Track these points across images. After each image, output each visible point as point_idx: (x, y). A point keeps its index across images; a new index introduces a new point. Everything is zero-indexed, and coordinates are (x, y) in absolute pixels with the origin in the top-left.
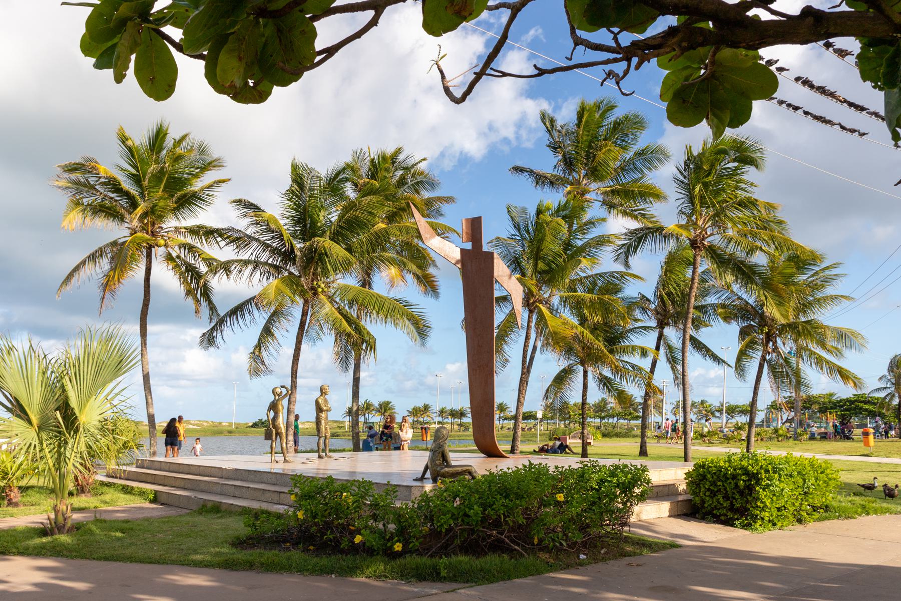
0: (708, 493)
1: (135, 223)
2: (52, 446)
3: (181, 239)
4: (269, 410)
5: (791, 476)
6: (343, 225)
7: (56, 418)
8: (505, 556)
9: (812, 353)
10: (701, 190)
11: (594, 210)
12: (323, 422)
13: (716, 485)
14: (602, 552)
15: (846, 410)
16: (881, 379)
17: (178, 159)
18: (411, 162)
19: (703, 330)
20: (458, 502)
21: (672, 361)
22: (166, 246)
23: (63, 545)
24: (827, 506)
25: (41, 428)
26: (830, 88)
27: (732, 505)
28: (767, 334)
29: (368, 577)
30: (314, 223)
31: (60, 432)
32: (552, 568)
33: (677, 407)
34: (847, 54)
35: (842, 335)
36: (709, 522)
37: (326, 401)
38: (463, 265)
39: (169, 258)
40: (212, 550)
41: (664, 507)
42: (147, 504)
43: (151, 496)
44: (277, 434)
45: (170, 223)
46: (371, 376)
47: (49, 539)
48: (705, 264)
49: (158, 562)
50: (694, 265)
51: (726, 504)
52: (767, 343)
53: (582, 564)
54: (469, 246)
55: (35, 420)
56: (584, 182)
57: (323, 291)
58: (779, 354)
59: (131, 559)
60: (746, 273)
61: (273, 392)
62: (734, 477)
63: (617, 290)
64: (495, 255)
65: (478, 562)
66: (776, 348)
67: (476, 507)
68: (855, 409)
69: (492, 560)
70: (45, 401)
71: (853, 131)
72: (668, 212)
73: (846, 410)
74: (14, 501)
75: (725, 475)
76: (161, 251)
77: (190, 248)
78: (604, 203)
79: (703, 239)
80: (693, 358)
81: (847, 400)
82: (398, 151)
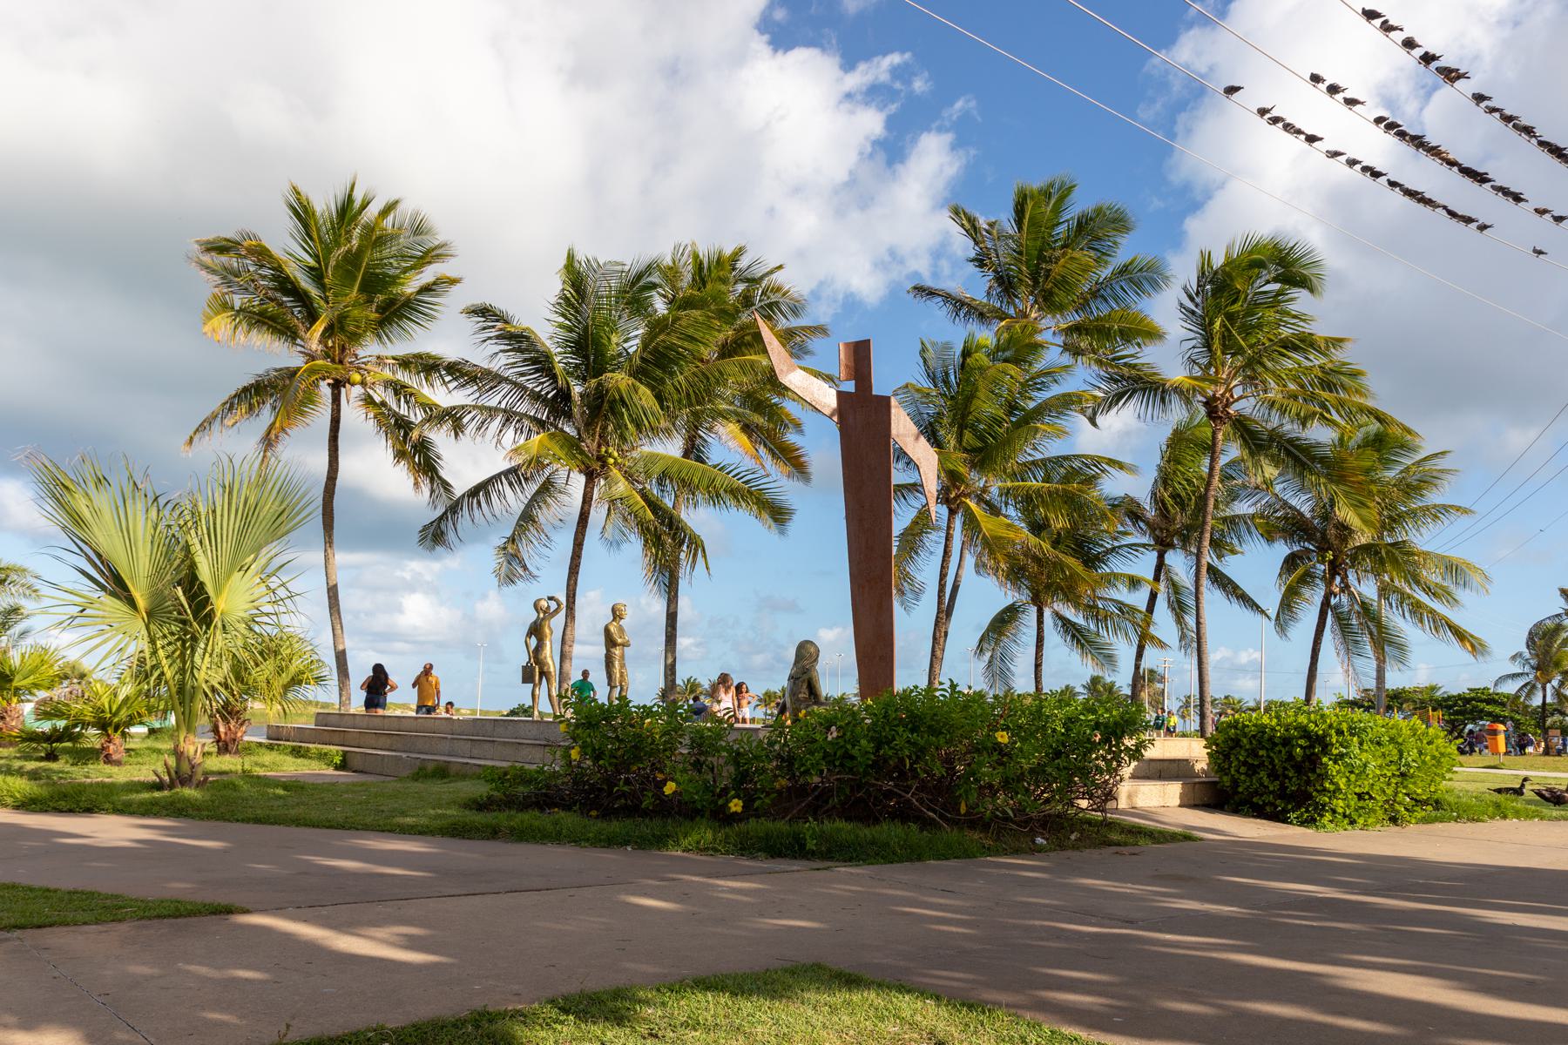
0: (1243, 769)
1: (314, 345)
2: (171, 648)
3: (387, 374)
4: (530, 634)
5: (1379, 743)
6: (649, 357)
7: (177, 599)
8: (914, 827)
9: (1404, 597)
10: (1223, 325)
11: (1052, 356)
12: (617, 664)
13: (1256, 756)
14: (1073, 837)
15: (1456, 713)
16: (1514, 658)
17: (381, 241)
18: (758, 272)
19: (1230, 558)
20: (834, 734)
21: (1178, 608)
22: (363, 383)
23: (187, 800)
24: (1437, 802)
25: (150, 614)
26: (1432, 140)
27: (1283, 787)
28: (1331, 562)
29: (686, 850)
30: (600, 350)
31: (184, 622)
32: (990, 851)
33: (1187, 705)
34: (1459, 77)
35: (1453, 569)
36: (1247, 815)
37: (621, 629)
38: (840, 417)
39: (368, 401)
40: (432, 812)
41: (1187, 618)
42: (331, 771)
43: (337, 760)
44: (542, 673)
45: (369, 349)
46: (698, 645)
47: (166, 793)
48: (1232, 451)
49: (342, 827)
50: (1211, 449)
51: (1274, 786)
52: (1333, 578)
53: (1040, 850)
54: (850, 387)
55: (142, 603)
56: (1033, 315)
57: (616, 463)
58: (1351, 594)
59: (298, 822)
60: (1298, 458)
61: (536, 606)
62: (1286, 741)
63: (1091, 481)
64: (894, 402)
65: (866, 832)
66: (1347, 586)
67: (864, 742)
68: (1472, 712)
69: (890, 831)
70: (158, 572)
71: (1468, 220)
72: (1171, 351)
73: (1456, 713)
74: (115, 757)
75: (1271, 739)
76: (357, 390)
77: (399, 389)
78: (1066, 347)
79: (1228, 405)
80: (1213, 597)
81: (1459, 697)
82: (739, 252)
